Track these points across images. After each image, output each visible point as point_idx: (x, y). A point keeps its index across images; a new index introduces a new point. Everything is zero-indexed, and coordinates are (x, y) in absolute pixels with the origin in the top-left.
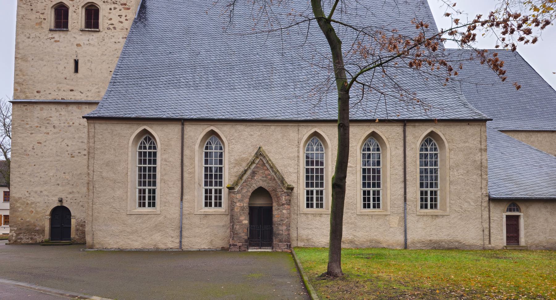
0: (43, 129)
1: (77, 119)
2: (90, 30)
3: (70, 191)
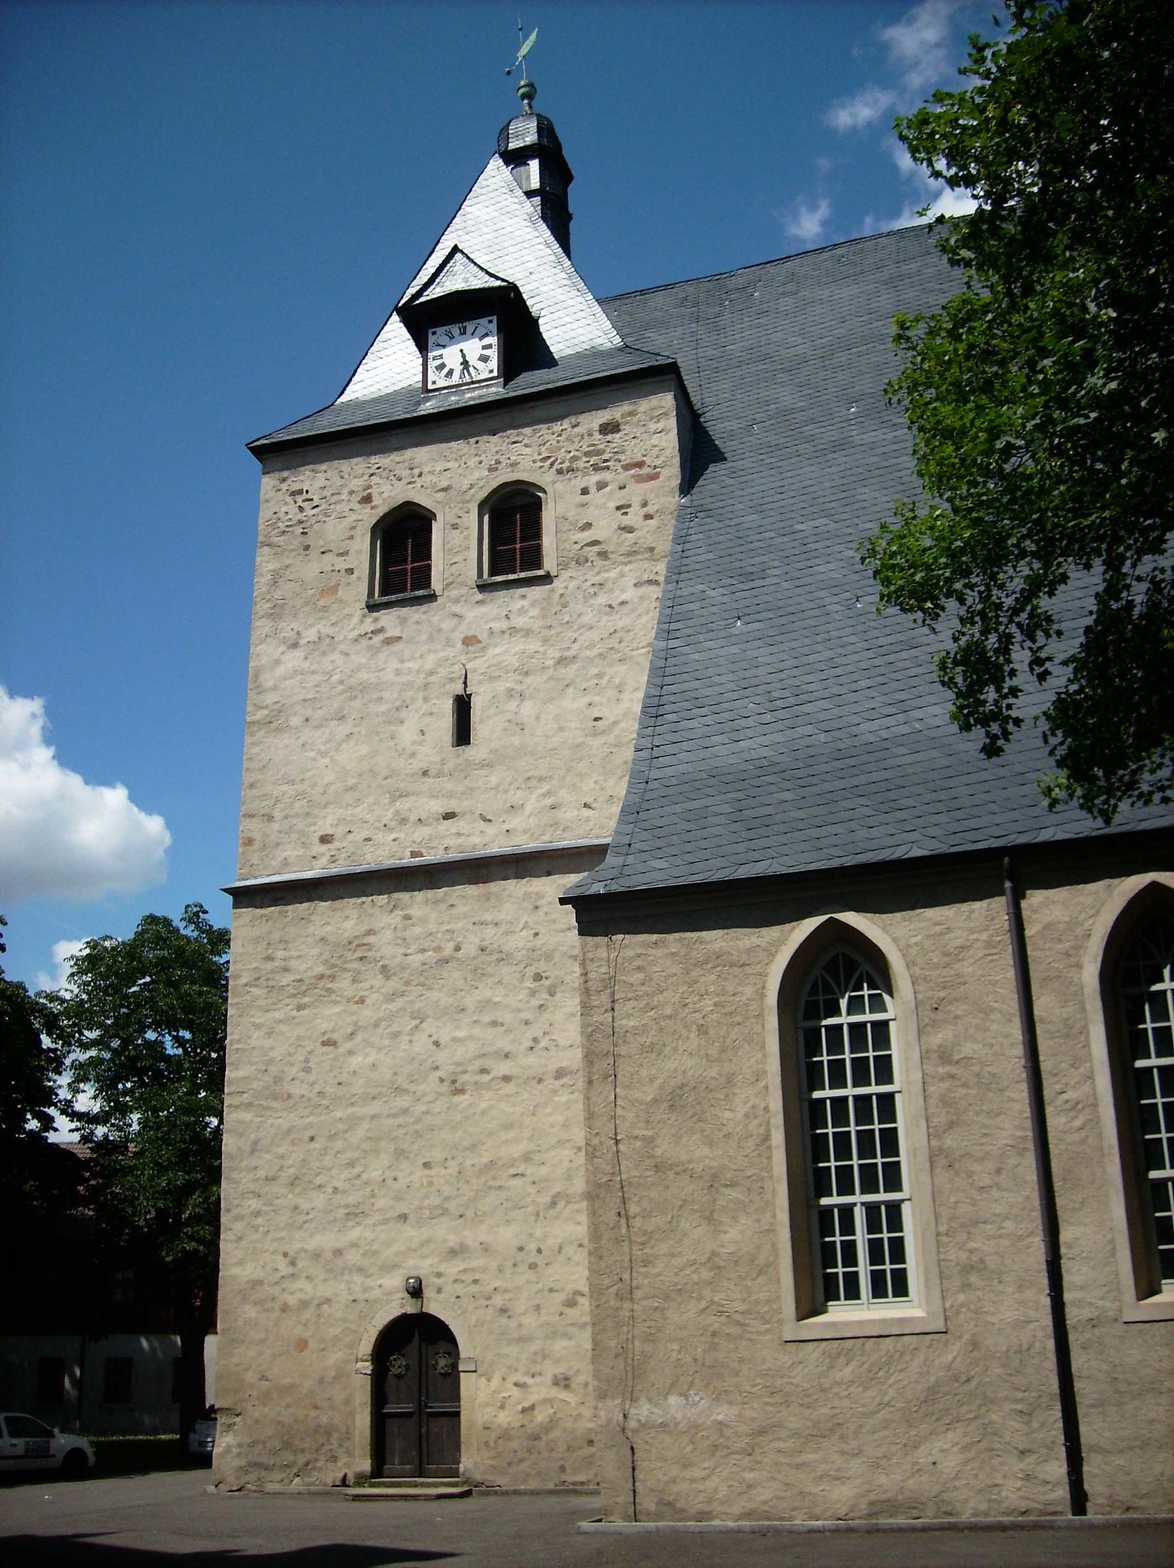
0: (343, 983)
1: (470, 927)
2: (512, 577)
3: (453, 1240)
